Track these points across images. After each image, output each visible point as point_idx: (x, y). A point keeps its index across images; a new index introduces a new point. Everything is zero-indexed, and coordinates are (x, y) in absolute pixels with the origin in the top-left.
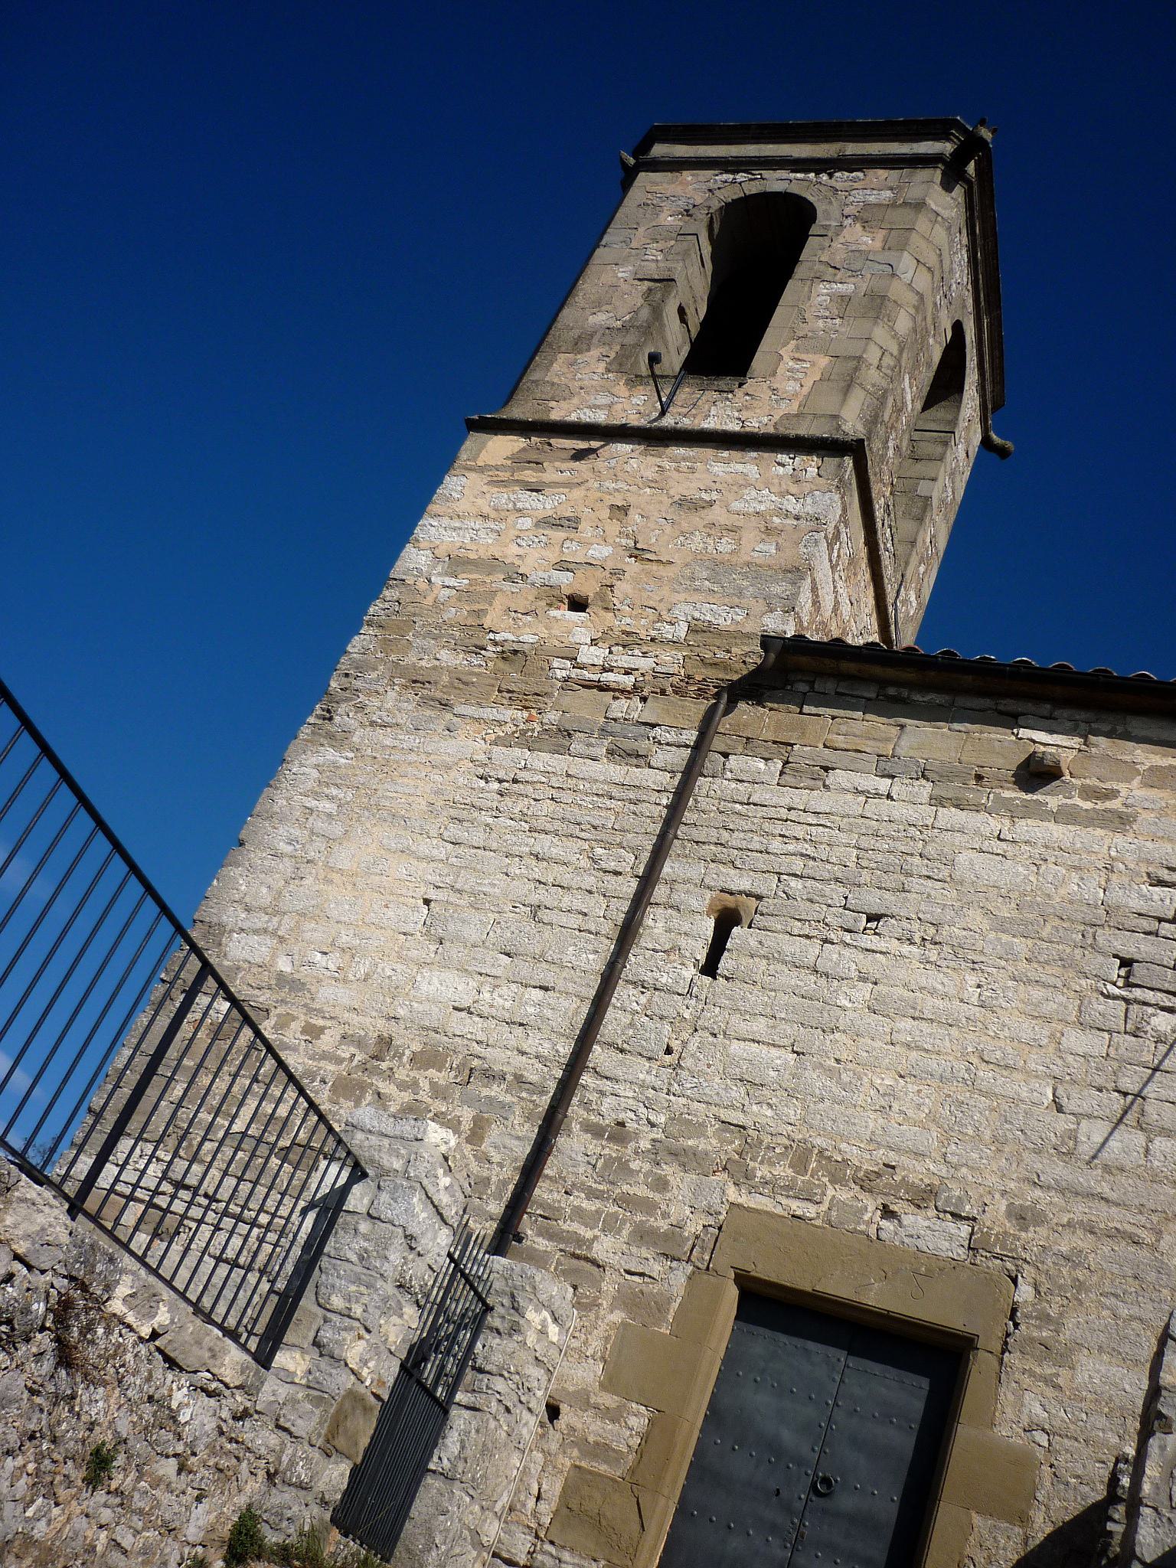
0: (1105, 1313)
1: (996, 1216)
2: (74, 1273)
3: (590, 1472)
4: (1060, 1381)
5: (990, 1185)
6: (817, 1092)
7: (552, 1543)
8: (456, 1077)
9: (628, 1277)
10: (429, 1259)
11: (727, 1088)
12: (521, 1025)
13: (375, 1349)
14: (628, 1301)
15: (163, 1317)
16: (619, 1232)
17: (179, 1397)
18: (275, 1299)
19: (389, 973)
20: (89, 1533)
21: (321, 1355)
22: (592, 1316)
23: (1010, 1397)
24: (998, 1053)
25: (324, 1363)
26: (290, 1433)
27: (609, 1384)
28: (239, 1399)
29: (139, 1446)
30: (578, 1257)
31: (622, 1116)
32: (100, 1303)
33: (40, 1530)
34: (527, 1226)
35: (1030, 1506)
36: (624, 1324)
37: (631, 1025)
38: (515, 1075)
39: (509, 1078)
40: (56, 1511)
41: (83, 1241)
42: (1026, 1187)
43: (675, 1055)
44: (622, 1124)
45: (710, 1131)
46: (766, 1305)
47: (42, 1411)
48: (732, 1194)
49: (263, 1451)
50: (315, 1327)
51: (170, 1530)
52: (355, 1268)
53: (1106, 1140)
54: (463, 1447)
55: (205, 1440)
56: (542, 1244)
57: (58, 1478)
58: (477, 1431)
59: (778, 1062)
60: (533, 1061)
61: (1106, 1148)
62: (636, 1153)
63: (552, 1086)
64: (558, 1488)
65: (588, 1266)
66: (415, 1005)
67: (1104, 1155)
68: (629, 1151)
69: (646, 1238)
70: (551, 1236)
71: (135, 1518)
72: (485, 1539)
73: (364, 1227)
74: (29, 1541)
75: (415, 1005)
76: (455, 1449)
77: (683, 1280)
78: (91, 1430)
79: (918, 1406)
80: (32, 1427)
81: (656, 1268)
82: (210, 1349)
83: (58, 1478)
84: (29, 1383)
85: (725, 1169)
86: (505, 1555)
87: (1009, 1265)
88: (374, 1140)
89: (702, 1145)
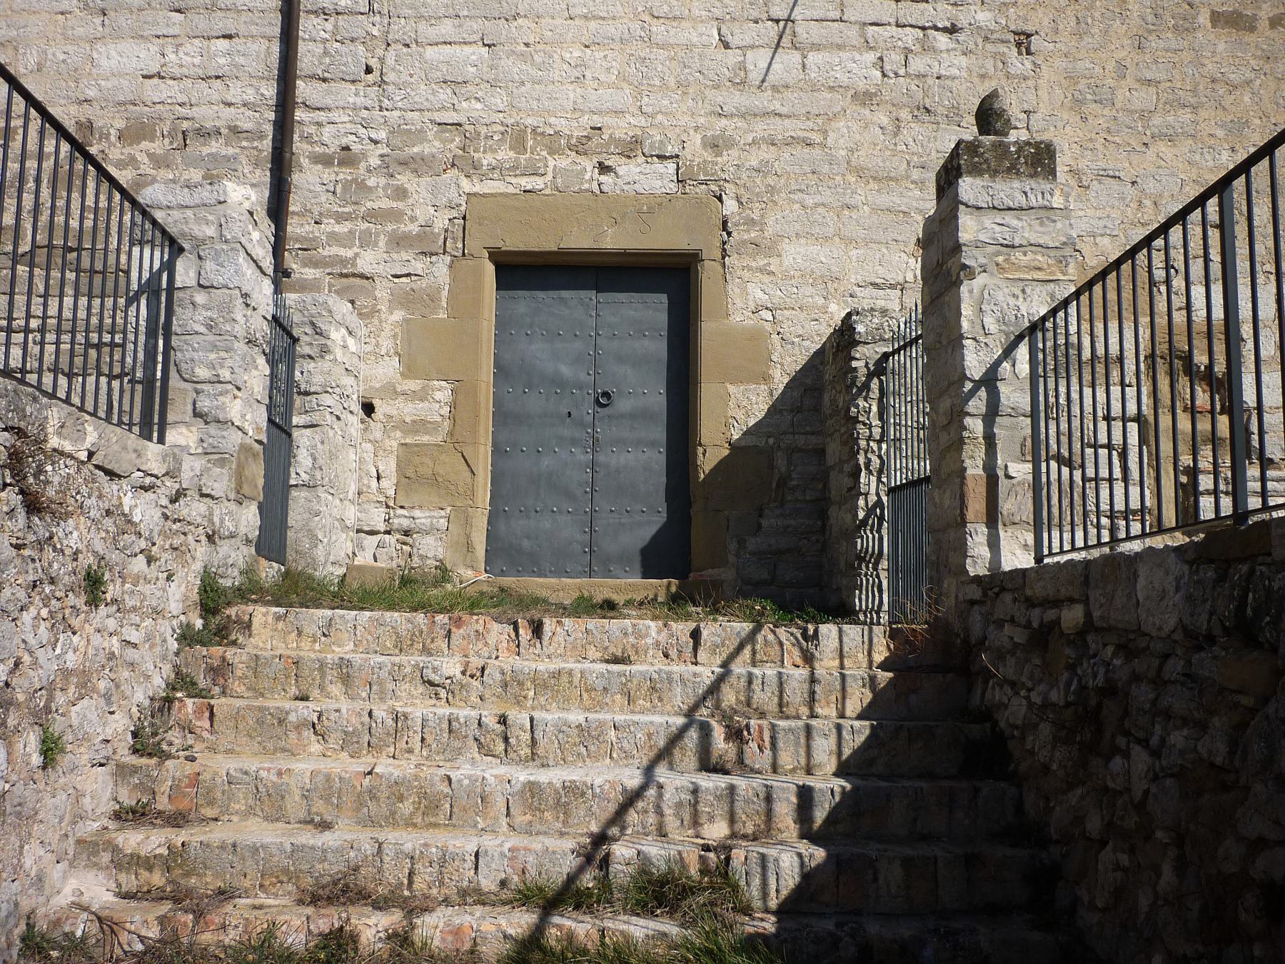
0: (797, 206)
1: (695, 151)
2: (10, 424)
3: (416, 445)
4: (772, 268)
5: (682, 122)
6: (517, 77)
7: (402, 507)
8: (171, 143)
9: (396, 280)
10: (261, 311)
11: (434, 93)
12: (217, 77)
13: (247, 402)
14: (405, 300)
15: (91, 437)
16: (376, 244)
17: (127, 501)
18: (139, 388)
19: (62, 57)
20: (106, 644)
21: (207, 423)
22: (376, 321)
23: (737, 290)
24: (665, 7)
25: (212, 429)
26: (212, 497)
27: (409, 371)
28: (168, 484)
29: (114, 557)
30: (346, 276)
31: (344, 141)
32: (40, 442)
33: (72, 660)
34: (290, 262)
35: (769, 367)
36: (406, 321)
37: (326, 53)
38: (229, 128)
39: (224, 131)
40: (76, 639)
41: (6, 390)
42: (713, 119)
43: (376, 73)
44: (347, 148)
45: (430, 135)
46: (517, 271)
47: (33, 560)
48: (467, 186)
49: (199, 520)
50: (190, 401)
51: (157, 613)
52: (206, 338)
53: (770, 64)
54: (315, 459)
55: (157, 529)
56: (310, 273)
57: (67, 611)
58: (322, 443)
59: (474, 57)
60: (242, 109)
61: (771, 71)
62: (369, 171)
63: (269, 129)
64: (393, 465)
65: (358, 281)
66: (103, 83)
67: (770, 77)
68: (362, 171)
69: (402, 243)
70: (315, 264)
71: (132, 616)
72: (348, 523)
73: (200, 298)
74: (66, 673)
75: (103, 83)
76: (309, 462)
77: (445, 270)
78: (76, 560)
79: (663, 318)
80: (31, 578)
81: (418, 266)
82: (135, 451)
83: (67, 611)
84: (14, 541)
85: (453, 165)
86: (367, 529)
87: (714, 188)
88: (176, 214)
89: (427, 149)
